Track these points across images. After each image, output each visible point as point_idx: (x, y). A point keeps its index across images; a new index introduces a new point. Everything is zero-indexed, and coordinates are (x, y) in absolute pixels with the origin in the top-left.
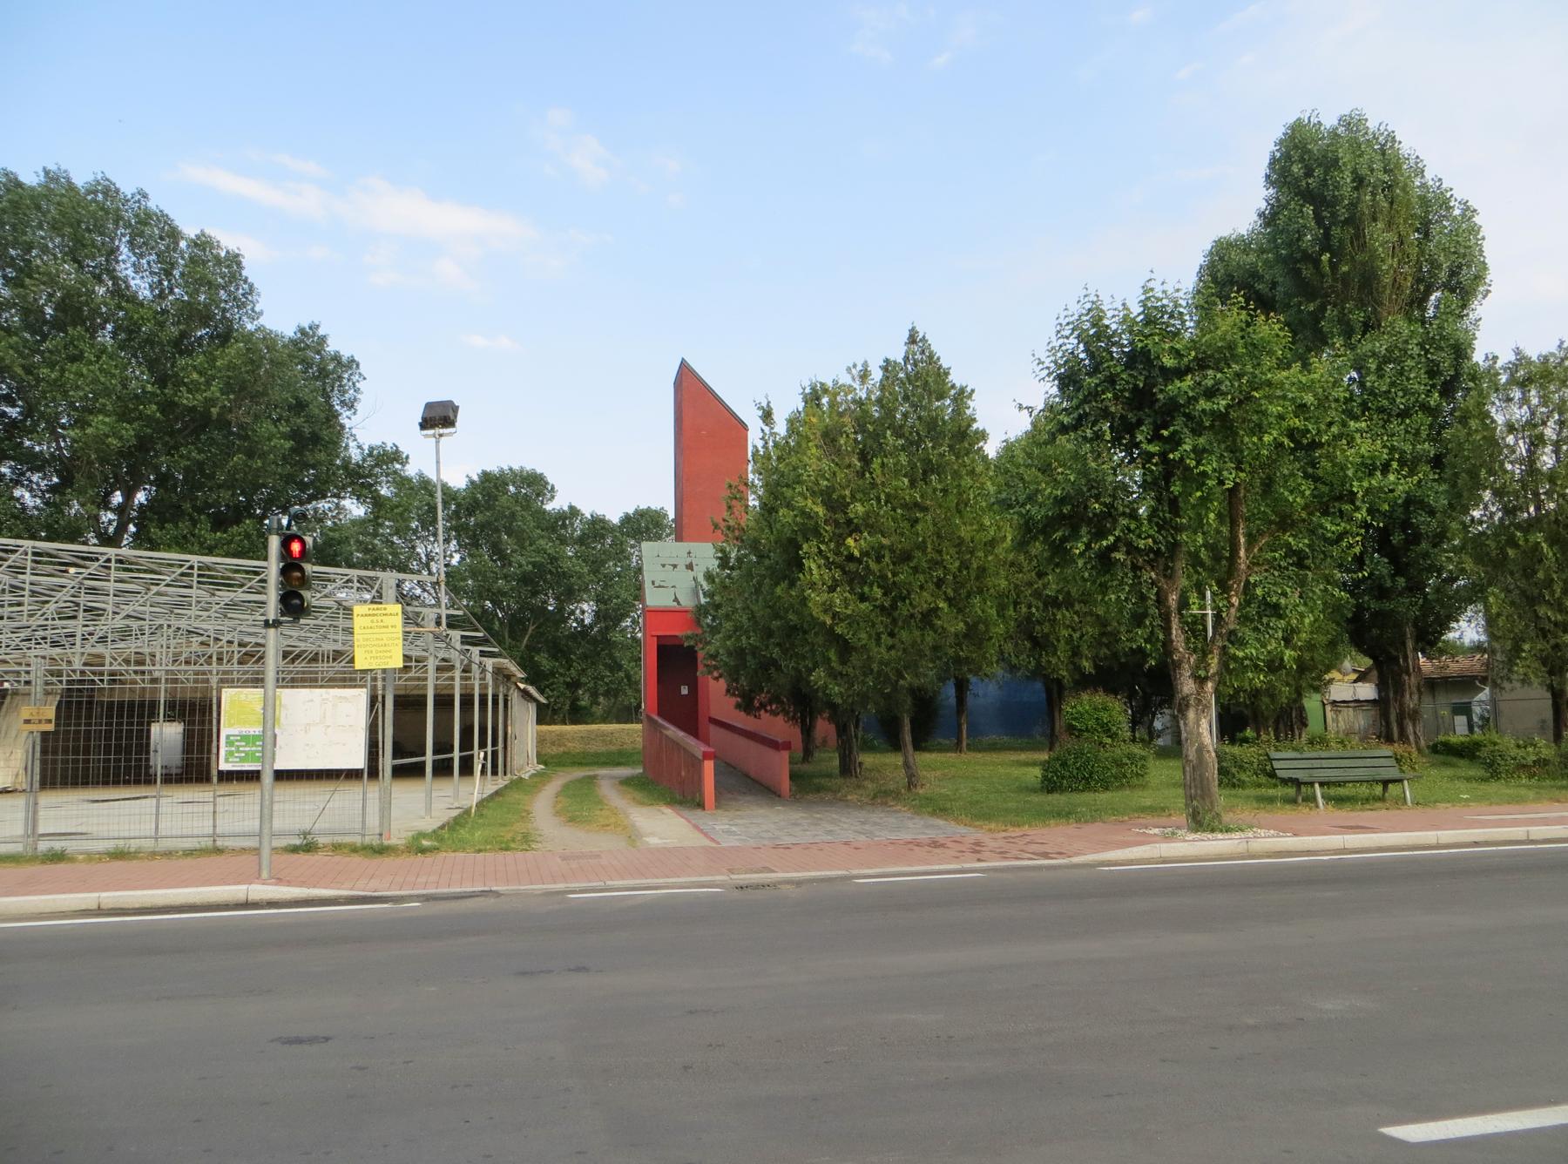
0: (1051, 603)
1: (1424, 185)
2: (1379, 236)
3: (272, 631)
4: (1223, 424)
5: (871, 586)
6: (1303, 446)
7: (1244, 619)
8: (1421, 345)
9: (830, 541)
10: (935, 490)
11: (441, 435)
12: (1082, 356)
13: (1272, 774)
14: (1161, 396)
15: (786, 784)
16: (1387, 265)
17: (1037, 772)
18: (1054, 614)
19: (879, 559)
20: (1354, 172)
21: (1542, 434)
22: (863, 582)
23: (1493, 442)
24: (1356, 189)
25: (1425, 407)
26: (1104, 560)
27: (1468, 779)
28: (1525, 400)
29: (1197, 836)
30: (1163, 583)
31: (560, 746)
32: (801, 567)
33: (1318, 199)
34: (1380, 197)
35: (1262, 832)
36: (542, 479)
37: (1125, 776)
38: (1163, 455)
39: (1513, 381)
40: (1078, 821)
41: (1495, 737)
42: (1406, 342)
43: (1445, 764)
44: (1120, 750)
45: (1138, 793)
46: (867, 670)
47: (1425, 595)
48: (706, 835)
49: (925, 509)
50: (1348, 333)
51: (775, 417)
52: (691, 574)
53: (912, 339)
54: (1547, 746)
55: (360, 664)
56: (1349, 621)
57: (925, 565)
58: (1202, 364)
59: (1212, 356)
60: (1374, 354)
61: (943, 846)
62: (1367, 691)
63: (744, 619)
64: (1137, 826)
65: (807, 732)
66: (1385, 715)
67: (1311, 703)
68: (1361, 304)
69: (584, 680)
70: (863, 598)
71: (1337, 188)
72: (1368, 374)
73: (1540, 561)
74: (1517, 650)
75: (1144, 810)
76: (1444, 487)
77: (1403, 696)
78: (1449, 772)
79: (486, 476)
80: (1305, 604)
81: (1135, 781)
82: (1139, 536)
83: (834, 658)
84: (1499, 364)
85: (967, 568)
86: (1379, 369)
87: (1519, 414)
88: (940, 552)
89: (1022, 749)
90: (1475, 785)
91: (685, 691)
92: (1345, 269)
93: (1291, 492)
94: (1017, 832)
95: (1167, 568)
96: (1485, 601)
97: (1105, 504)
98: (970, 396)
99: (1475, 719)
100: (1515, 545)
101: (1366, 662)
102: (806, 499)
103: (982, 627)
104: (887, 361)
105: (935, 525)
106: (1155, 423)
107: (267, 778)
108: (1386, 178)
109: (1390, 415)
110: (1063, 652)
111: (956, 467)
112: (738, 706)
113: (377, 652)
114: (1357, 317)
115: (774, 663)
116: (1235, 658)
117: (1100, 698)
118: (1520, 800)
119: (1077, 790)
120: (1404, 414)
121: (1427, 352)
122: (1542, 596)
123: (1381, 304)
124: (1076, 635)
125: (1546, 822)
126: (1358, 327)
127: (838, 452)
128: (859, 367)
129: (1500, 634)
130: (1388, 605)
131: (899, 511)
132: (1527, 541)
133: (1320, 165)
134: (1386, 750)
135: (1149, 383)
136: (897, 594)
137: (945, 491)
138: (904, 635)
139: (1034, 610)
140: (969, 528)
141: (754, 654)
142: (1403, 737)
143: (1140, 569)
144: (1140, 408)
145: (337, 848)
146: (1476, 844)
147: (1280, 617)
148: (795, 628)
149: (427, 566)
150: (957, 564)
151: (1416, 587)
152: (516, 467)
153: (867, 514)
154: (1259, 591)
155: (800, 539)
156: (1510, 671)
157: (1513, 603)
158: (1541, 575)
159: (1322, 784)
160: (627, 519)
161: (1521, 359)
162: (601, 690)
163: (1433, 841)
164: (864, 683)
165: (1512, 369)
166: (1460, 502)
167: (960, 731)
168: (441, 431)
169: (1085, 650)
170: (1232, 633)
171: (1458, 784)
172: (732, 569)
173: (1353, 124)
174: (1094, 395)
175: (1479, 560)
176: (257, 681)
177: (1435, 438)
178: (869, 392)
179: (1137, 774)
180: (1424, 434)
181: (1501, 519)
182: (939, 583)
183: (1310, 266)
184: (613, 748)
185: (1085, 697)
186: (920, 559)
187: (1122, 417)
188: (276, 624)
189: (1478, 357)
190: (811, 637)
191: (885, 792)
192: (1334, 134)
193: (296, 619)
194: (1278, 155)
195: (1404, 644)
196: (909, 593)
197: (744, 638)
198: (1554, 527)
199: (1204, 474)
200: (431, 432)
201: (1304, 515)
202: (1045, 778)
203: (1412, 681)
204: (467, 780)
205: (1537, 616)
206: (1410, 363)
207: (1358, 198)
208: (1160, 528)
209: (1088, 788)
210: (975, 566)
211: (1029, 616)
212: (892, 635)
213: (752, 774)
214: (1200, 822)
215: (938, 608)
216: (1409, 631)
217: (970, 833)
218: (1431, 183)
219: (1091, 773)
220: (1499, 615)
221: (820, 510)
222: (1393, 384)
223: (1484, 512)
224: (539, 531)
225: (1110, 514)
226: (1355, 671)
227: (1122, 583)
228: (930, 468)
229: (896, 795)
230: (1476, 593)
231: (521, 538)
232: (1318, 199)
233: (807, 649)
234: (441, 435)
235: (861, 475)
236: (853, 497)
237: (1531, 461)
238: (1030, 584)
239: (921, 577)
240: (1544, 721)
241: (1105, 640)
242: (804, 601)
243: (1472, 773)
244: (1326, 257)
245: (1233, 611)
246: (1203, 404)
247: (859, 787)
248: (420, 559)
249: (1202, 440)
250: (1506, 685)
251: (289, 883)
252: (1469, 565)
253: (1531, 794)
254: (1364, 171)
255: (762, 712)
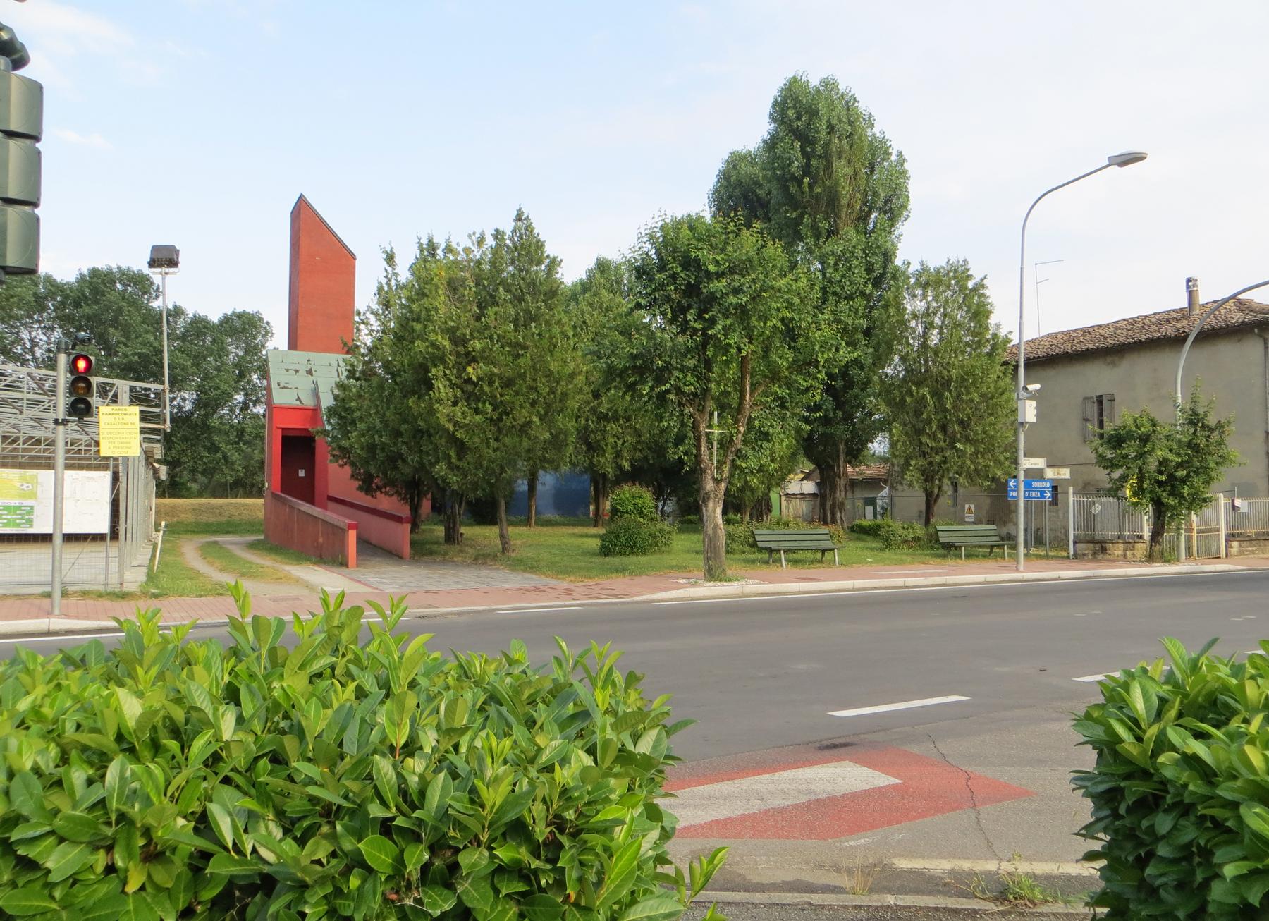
0: (604, 418)
1: (874, 135)
2: (842, 169)
3: (61, 428)
4: (743, 313)
5: (484, 403)
6: (790, 333)
7: (745, 442)
8: (863, 250)
9: (453, 367)
10: (533, 334)
11: (166, 273)
12: (654, 256)
13: (754, 545)
14: (705, 291)
15: (407, 550)
16: (846, 191)
17: (598, 542)
18: (604, 426)
19: (491, 383)
20: (829, 121)
21: (932, 322)
22: (478, 399)
23: (903, 323)
24: (829, 133)
25: (863, 294)
26: (662, 397)
27: (872, 549)
28: (924, 296)
29: (711, 584)
30: (697, 416)
31: (173, 516)
32: (430, 387)
33: (804, 138)
34: (844, 142)
35: (750, 581)
36: (148, 280)
37: (657, 545)
38: (704, 331)
39: (918, 284)
40: (631, 574)
41: (890, 522)
42: (854, 247)
43: (858, 539)
44: (654, 528)
45: (666, 556)
46: (479, 465)
47: (854, 425)
48: (365, 585)
49: (525, 348)
50: (817, 236)
51: (397, 259)
52: (311, 378)
53: (519, 218)
54: (921, 529)
55: (105, 451)
56: (805, 440)
57: (524, 390)
58: (732, 271)
59: (738, 266)
60: (833, 254)
61: (544, 591)
62: (809, 487)
63: (377, 422)
64: (671, 577)
65: (415, 508)
66: (823, 505)
67: (774, 496)
68: (827, 218)
69: (184, 459)
70: (477, 411)
71: (817, 131)
72: (828, 267)
73: (925, 406)
74: (907, 464)
75: (672, 567)
76: (871, 350)
77: (835, 492)
78: (861, 544)
79: (95, 273)
80: (784, 433)
81: (664, 548)
82: (685, 384)
83: (453, 455)
84: (911, 270)
85: (553, 393)
86: (836, 264)
87: (920, 305)
88: (534, 380)
89: (574, 525)
90: (876, 552)
91: (302, 473)
92: (818, 190)
93: (780, 358)
94: (590, 582)
95: (700, 405)
96: (890, 431)
97: (664, 361)
98: (559, 265)
99: (878, 509)
100: (911, 395)
101: (809, 467)
102: (437, 334)
103: (562, 436)
104: (497, 230)
105: (532, 360)
106: (699, 308)
107: (58, 540)
108: (849, 128)
109: (840, 297)
110: (609, 454)
111: (547, 317)
112: (360, 488)
113: (119, 443)
114: (824, 225)
115: (400, 456)
116: (739, 467)
117: (636, 489)
118: (901, 562)
119: (625, 554)
120: (849, 298)
121: (867, 255)
122: (924, 429)
123: (839, 218)
124: (620, 442)
125: (915, 575)
126: (824, 233)
127: (460, 300)
128: (478, 235)
129: (897, 453)
130: (830, 430)
131: (507, 349)
132: (918, 392)
133: (806, 113)
134: (825, 530)
135: (698, 282)
136: (504, 411)
137: (539, 335)
138: (507, 440)
139: (590, 422)
140: (556, 364)
141: (383, 449)
142: (834, 521)
143: (684, 405)
144: (690, 297)
145: (85, 594)
146: (875, 588)
147: (768, 441)
148: (421, 431)
149: (32, 351)
150: (547, 390)
151: (848, 418)
152: (124, 266)
153: (483, 350)
154: (757, 424)
155: (429, 364)
156: (902, 478)
157: (906, 434)
158: (925, 416)
159: (785, 551)
160: (226, 320)
161: (924, 269)
162: (200, 469)
163: (851, 587)
164: (475, 475)
165: (919, 274)
166: (880, 359)
167: (530, 510)
168: (167, 270)
169: (626, 455)
170: (739, 451)
171: (868, 553)
172: (357, 379)
173: (829, 85)
174: (662, 286)
175: (889, 404)
176: (50, 466)
177: (867, 316)
178: (484, 253)
179: (665, 544)
180: (861, 312)
181: (904, 376)
182: (533, 403)
183: (795, 185)
184: (221, 519)
185: (626, 488)
186: (522, 385)
187: (679, 302)
188: (65, 422)
189: (898, 261)
190: (435, 439)
191: (483, 555)
192: (817, 90)
193: (80, 420)
194: (779, 99)
195: (838, 457)
196: (512, 410)
197: (376, 437)
198: (935, 384)
199: (729, 345)
200: (158, 270)
201: (787, 373)
202: (603, 546)
203: (841, 482)
204: (115, 543)
205: (921, 443)
206: (855, 262)
207: (830, 140)
208: (699, 378)
209: (632, 553)
210: (559, 392)
211: (586, 428)
212: (497, 439)
213: (374, 542)
214: (712, 574)
215: (531, 422)
216: (842, 447)
217: (562, 583)
218: (878, 135)
219: (635, 543)
220: (898, 441)
221: (447, 344)
222: (843, 276)
223: (893, 369)
224: (146, 326)
225: (668, 368)
226: (802, 472)
227: (671, 414)
228: (532, 318)
229: (494, 558)
230: (884, 425)
231: (127, 331)
232: (804, 138)
233: (431, 447)
234: (166, 273)
235: (478, 318)
236: (471, 334)
237: (924, 339)
238: (588, 403)
239: (521, 398)
240: (921, 512)
241: (639, 447)
242: (432, 412)
243: (875, 545)
244: (806, 180)
245: (740, 436)
246: (732, 299)
247: (461, 551)
248: (24, 344)
249: (728, 322)
250: (899, 487)
251: (77, 617)
252: (882, 407)
253: (909, 559)
254: (835, 121)
255: (378, 493)
